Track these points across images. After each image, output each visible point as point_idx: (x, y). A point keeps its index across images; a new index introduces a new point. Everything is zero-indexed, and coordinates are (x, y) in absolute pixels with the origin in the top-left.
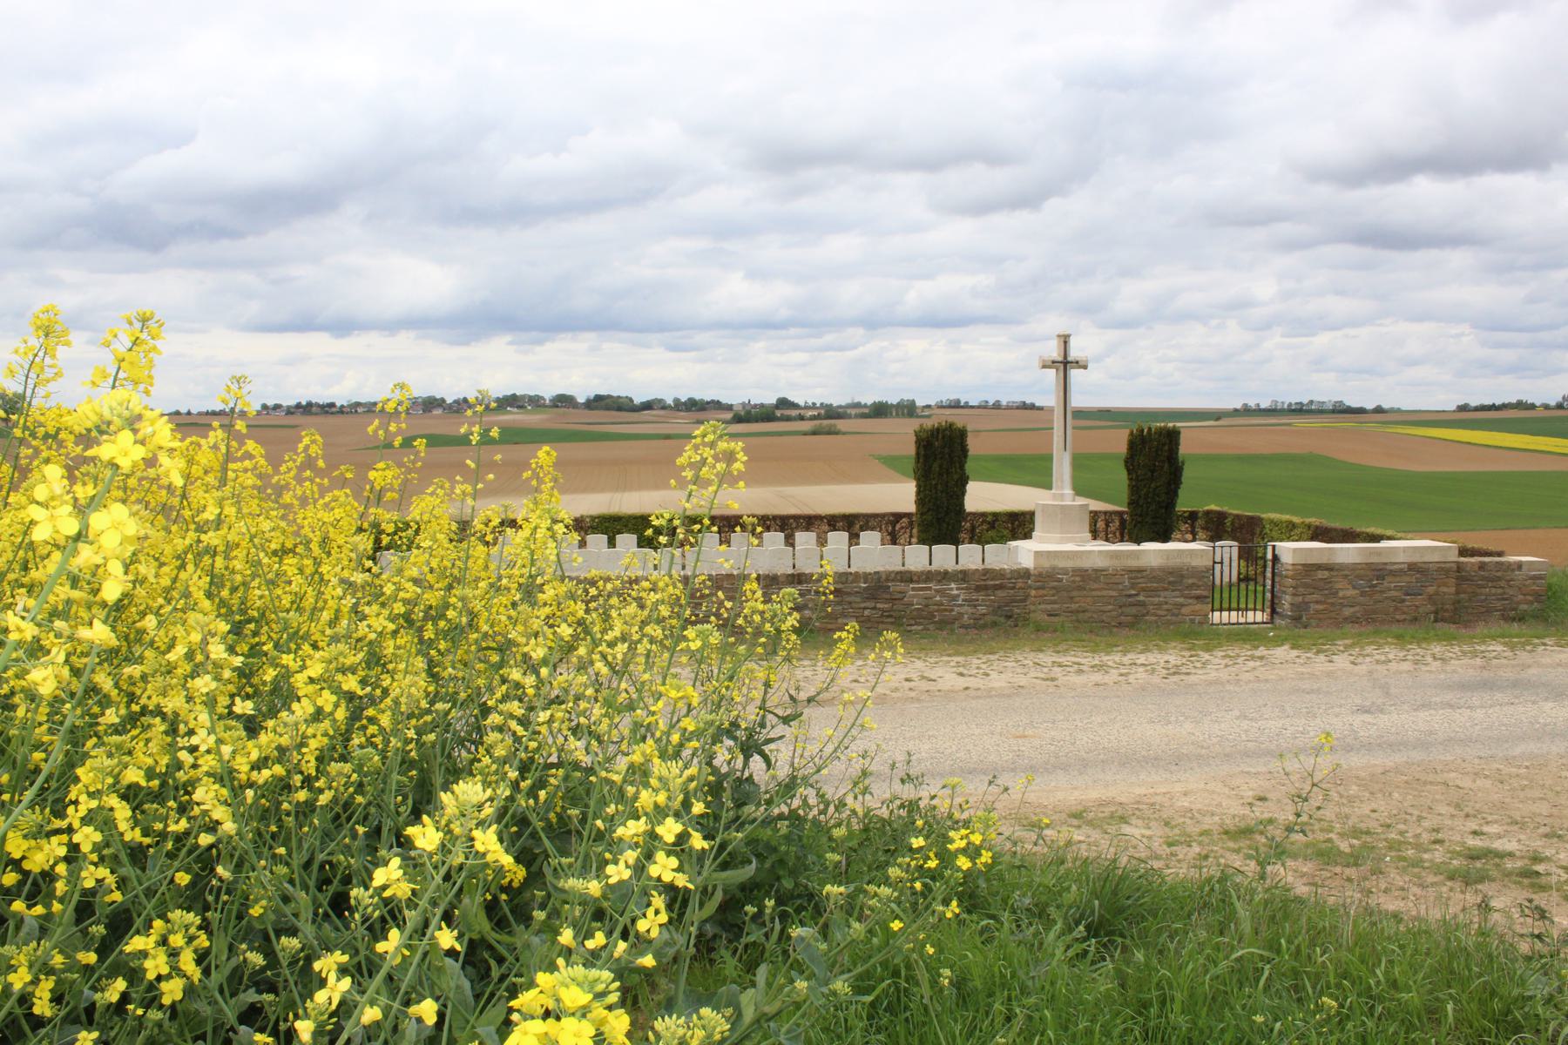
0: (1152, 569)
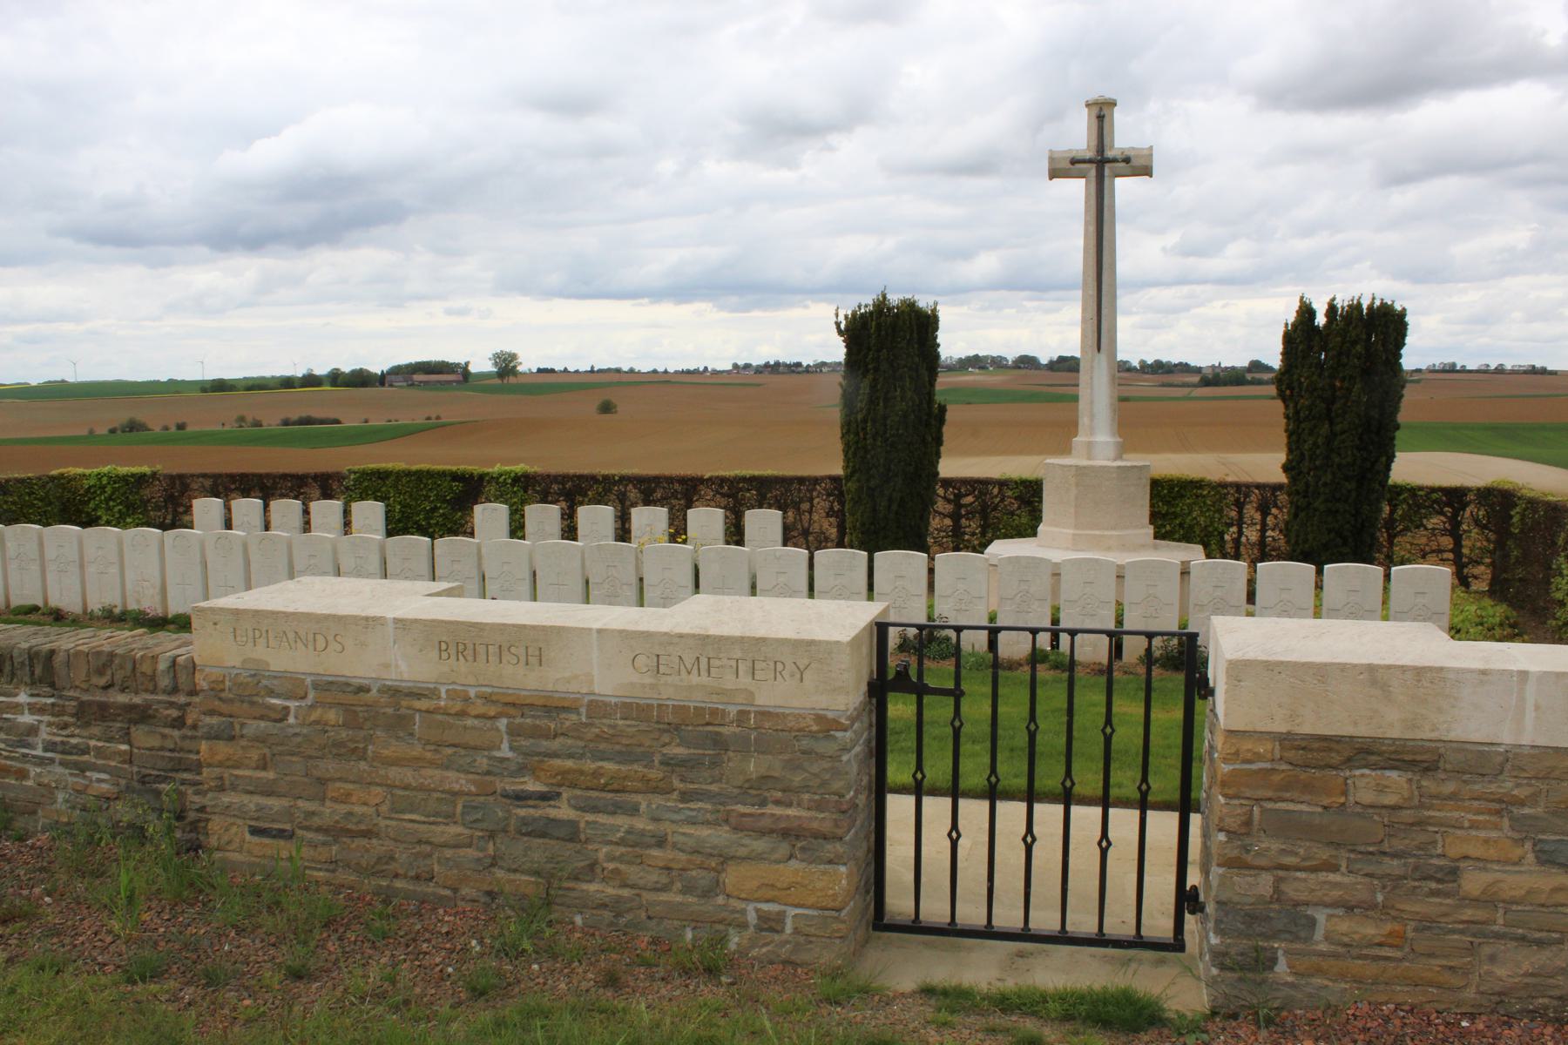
0: (598, 708)
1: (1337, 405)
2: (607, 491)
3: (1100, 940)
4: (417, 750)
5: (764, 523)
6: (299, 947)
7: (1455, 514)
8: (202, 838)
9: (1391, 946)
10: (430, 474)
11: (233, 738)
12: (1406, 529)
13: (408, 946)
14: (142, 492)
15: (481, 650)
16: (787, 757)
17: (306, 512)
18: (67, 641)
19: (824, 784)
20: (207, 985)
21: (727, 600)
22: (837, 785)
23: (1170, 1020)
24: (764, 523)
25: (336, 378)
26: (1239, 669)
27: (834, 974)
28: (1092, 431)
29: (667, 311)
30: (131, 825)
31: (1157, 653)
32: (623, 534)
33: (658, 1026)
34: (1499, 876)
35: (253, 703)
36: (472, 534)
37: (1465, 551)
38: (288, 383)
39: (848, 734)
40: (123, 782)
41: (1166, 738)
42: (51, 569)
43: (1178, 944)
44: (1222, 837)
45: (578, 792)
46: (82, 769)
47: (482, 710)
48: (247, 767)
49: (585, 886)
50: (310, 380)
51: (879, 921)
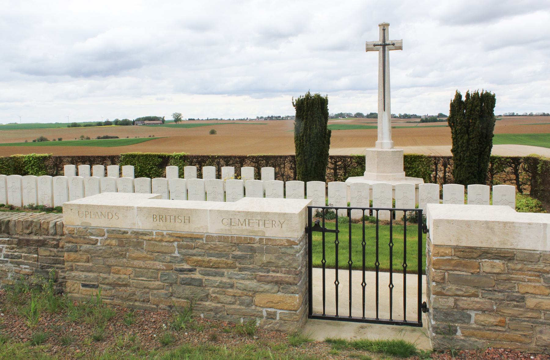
0: (210, 238)
1: (470, 129)
2: (213, 161)
3: (390, 322)
4: (145, 254)
5: (268, 172)
6: (99, 329)
7: (516, 167)
8: (63, 288)
9: (500, 326)
10: (150, 156)
11: (76, 251)
12: (498, 172)
13: (139, 327)
14: (45, 163)
15: (168, 218)
16: (276, 255)
17: (106, 169)
18: (14, 217)
19: (290, 264)
20: (63, 345)
21: (255, 199)
22: (295, 265)
23: (418, 353)
24: (268, 172)
25: (117, 123)
26: (438, 223)
27: (295, 335)
28: (382, 139)
29: (234, 99)
30: (37, 285)
31: (408, 217)
32: (219, 176)
33: (231, 355)
34: (540, 300)
35: (84, 238)
36: (165, 177)
37: (520, 180)
38: (99, 124)
39: (299, 246)
40: (34, 269)
41: (412, 247)
42: (9, 191)
43: (419, 324)
44: (434, 284)
45: (203, 268)
46: (18, 264)
47: (168, 239)
48: (82, 262)
49: (204, 303)
50: (108, 123)
51: (311, 315)
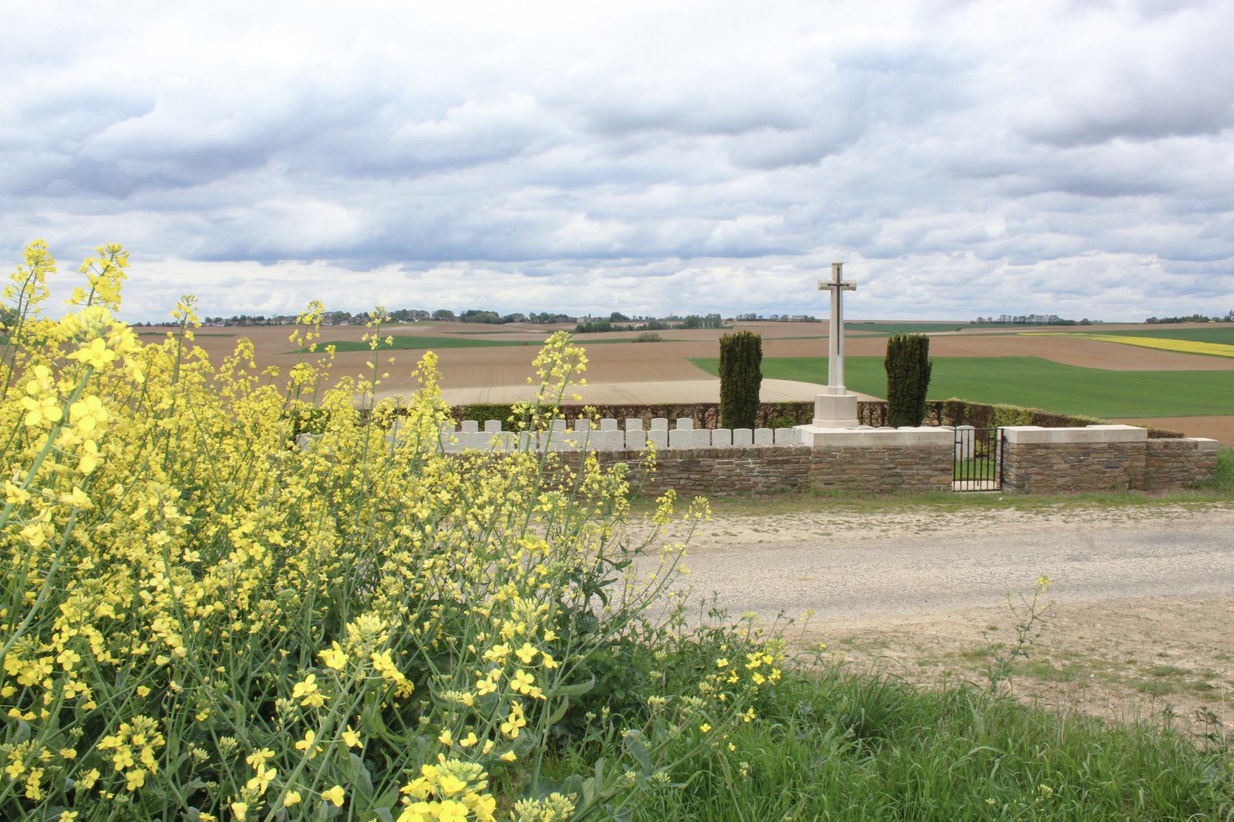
0: (907, 448)
